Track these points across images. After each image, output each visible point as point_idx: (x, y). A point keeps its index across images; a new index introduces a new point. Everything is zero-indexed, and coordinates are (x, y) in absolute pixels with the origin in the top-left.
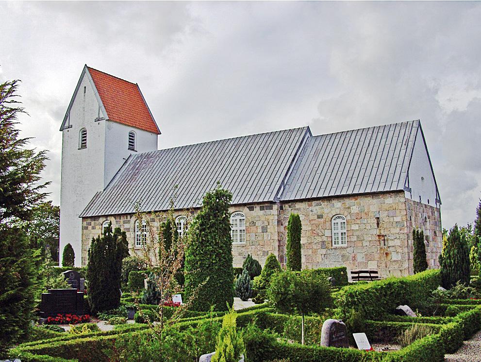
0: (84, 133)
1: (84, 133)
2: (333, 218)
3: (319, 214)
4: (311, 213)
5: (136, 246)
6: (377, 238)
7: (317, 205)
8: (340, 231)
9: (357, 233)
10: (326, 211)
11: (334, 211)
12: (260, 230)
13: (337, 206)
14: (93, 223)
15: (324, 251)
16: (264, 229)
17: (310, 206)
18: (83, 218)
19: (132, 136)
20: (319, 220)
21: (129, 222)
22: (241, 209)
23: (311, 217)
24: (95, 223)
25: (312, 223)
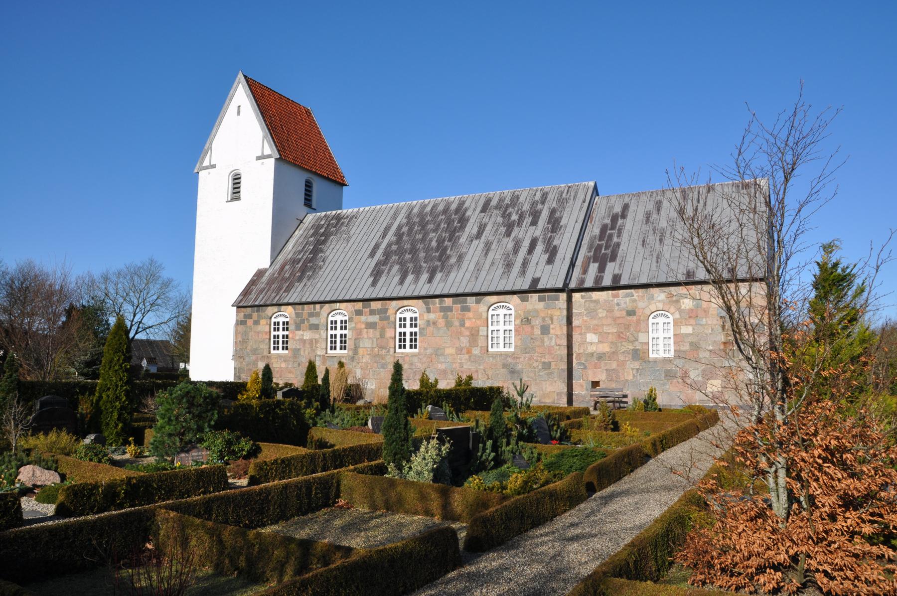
0: (237, 180)
1: (237, 180)
2: (492, 307)
3: (630, 308)
4: (616, 308)
5: (329, 351)
6: (722, 347)
7: (627, 296)
8: (501, 327)
9: (690, 339)
10: (641, 305)
11: (654, 305)
12: (537, 331)
13: (659, 298)
14: (255, 315)
15: (636, 365)
16: (545, 330)
17: (614, 296)
18: (238, 307)
19: (308, 186)
20: (630, 318)
21: (318, 315)
22: (508, 297)
23: (617, 314)
24: (259, 316)
25: (618, 322)
